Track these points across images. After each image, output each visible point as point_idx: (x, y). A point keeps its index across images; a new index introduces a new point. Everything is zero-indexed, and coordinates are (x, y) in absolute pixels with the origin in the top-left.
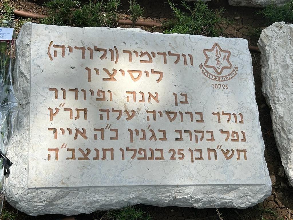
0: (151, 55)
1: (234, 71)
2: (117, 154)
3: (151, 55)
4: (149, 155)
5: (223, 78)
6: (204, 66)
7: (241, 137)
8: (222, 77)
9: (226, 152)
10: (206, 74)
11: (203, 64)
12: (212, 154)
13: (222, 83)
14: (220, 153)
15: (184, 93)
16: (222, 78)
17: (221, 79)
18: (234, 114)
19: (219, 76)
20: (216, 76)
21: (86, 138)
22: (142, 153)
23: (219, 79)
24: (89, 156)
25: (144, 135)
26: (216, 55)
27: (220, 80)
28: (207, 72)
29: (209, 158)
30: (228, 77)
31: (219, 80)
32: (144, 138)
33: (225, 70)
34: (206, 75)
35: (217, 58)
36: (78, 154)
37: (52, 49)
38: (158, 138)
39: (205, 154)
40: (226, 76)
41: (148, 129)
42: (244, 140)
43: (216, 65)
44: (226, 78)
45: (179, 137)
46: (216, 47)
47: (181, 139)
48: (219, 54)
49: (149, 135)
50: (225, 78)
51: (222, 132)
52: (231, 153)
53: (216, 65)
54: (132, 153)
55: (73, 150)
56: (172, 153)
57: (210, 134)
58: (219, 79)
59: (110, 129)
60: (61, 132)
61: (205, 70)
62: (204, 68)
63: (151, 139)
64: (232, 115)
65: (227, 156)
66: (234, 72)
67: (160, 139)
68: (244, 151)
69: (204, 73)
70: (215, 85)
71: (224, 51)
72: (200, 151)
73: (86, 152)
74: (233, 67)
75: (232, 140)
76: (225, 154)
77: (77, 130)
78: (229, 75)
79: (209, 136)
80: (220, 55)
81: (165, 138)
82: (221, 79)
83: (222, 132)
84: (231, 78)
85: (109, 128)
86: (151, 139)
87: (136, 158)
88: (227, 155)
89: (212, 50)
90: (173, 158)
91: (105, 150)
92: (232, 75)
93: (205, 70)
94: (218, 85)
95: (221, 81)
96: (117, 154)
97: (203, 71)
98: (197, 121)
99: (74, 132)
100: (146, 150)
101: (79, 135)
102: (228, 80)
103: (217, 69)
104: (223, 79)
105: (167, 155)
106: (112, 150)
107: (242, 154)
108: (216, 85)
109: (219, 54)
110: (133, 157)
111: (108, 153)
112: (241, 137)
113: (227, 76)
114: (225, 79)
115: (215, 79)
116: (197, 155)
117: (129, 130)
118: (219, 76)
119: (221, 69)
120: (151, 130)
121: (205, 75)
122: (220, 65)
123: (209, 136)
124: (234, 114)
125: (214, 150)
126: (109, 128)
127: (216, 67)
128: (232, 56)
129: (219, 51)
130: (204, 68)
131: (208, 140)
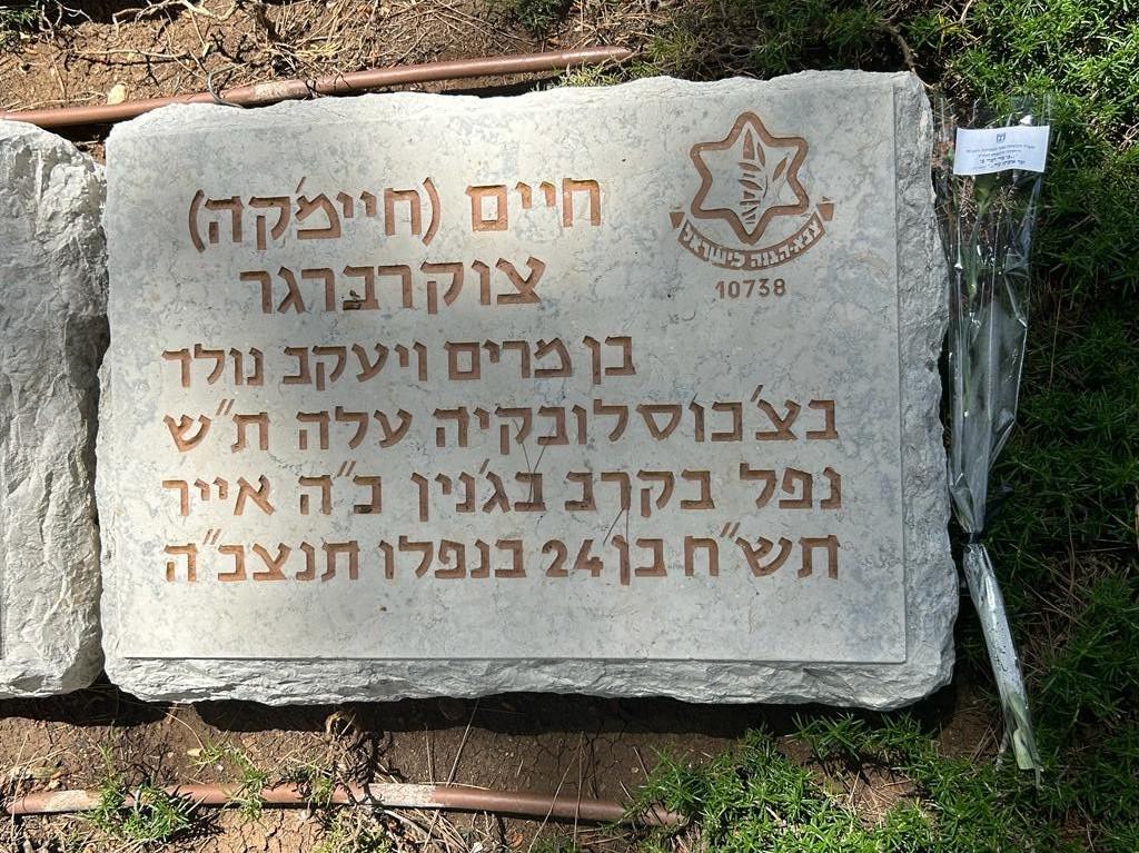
0: (339, 206)
1: (814, 222)
2: (371, 561)
3: (339, 206)
4: (473, 559)
5: (765, 255)
6: (688, 216)
7: (822, 491)
8: (761, 251)
9: (756, 547)
10: (695, 244)
11: (687, 209)
12: (702, 553)
13: (756, 275)
14: (729, 551)
15: (619, 333)
16: (758, 257)
17: (756, 260)
18: (233, 352)
19: (747, 247)
20: (733, 251)
21: (269, 509)
22: (448, 558)
23: (748, 260)
24: (283, 569)
25: (470, 495)
26: (747, 161)
27: (753, 264)
28: (700, 236)
29: (689, 570)
30: (785, 248)
31: (746, 266)
32: (467, 506)
33: (722, 224)
34: (697, 250)
35: (754, 177)
36: (253, 563)
37: (205, 217)
38: (511, 502)
39: (674, 556)
40: (775, 248)
41: (482, 470)
42: (834, 501)
43: (742, 203)
44: (778, 254)
45: (580, 499)
46: (744, 131)
47: (588, 502)
48: (757, 156)
49: (484, 490)
50: (772, 253)
51: (746, 472)
52: (777, 550)
53: (742, 203)
54: (419, 555)
55: (238, 550)
56: (554, 554)
57: (698, 483)
58: (748, 260)
59: (352, 476)
60: (199, 490)
61: (692, 228)
62: (688, 221)
63: (488, 507)
64: (227, 355)
65: (757, 564)
66: (814, 226)
67: (519, 506)
68: (831, 542)
69: (686, 245)
70: (731, 284)
71: (779, 142)
72: (656, 544)
73: (783, 413)
74: (813, 204)
75: (784, 504)
76: (752, 556)
77: (243, 485)
78: (790, 242)
79: (693, 490)
80: (762, 157)
81: (536, 504)
82: (756, 260)
83: (746, 472)
84: (797, 251)
85: (348, 475)
86: (488, 507)
87: (430, 572)
88: (759, 561)
89: (726, 143)
90: (556, 570)
91: (332, 549)
92: (805, 238)
93: (692, 228)
94: (741, 285)
95: (756, 268)
96: (371, 561)
97: (684, 232)
98: (717, 437)
99: (234, 490)
100: (463, 546)
101: (249, 501)
102: (787, 259)
103: (742, 219)
104: (763, 259)
105: (536, 562)
106: (352, 546)
107: (820, 555)
108: (734, 286)
109: (757, 156)
110: (421, 570)
111: (342, 559)
112: (822, 491)
113: (783, 244)
114: (770, 258)
115: (728, 265)
116: (645, 558)
117: (416, 477)
118: (747, 247)
119: (757, 221)
120: (491, 476)
121: (692, 250)
122: (759, 202)
123: (693, 490)
124: (233, 352)
125: (710, 543)
126: (348, 475)
127: (739, 210)
128: (967, 154)
129: (759, 144)
130: (688, 221)
131: (686, 504)
